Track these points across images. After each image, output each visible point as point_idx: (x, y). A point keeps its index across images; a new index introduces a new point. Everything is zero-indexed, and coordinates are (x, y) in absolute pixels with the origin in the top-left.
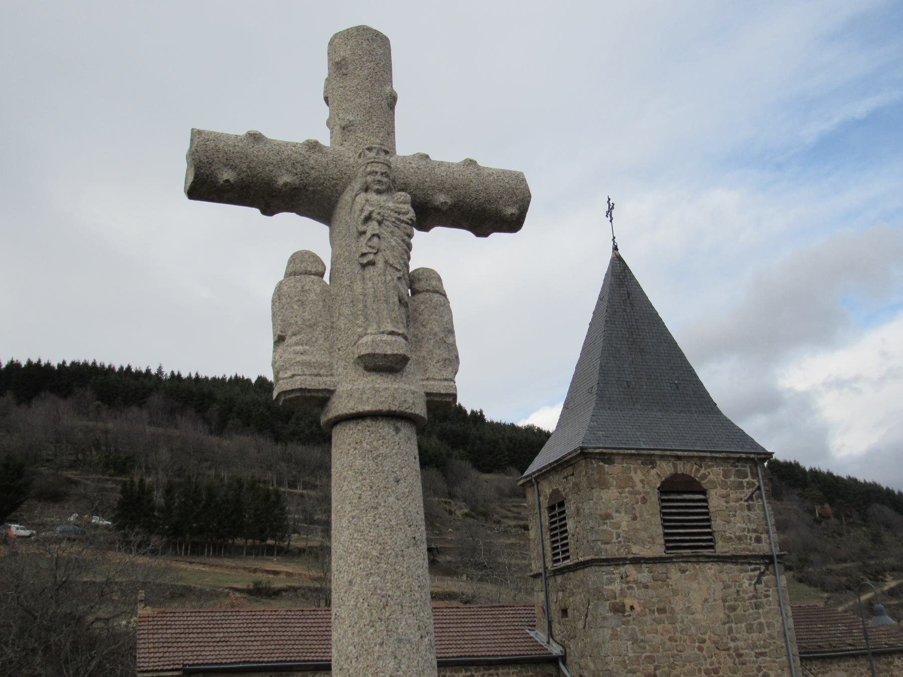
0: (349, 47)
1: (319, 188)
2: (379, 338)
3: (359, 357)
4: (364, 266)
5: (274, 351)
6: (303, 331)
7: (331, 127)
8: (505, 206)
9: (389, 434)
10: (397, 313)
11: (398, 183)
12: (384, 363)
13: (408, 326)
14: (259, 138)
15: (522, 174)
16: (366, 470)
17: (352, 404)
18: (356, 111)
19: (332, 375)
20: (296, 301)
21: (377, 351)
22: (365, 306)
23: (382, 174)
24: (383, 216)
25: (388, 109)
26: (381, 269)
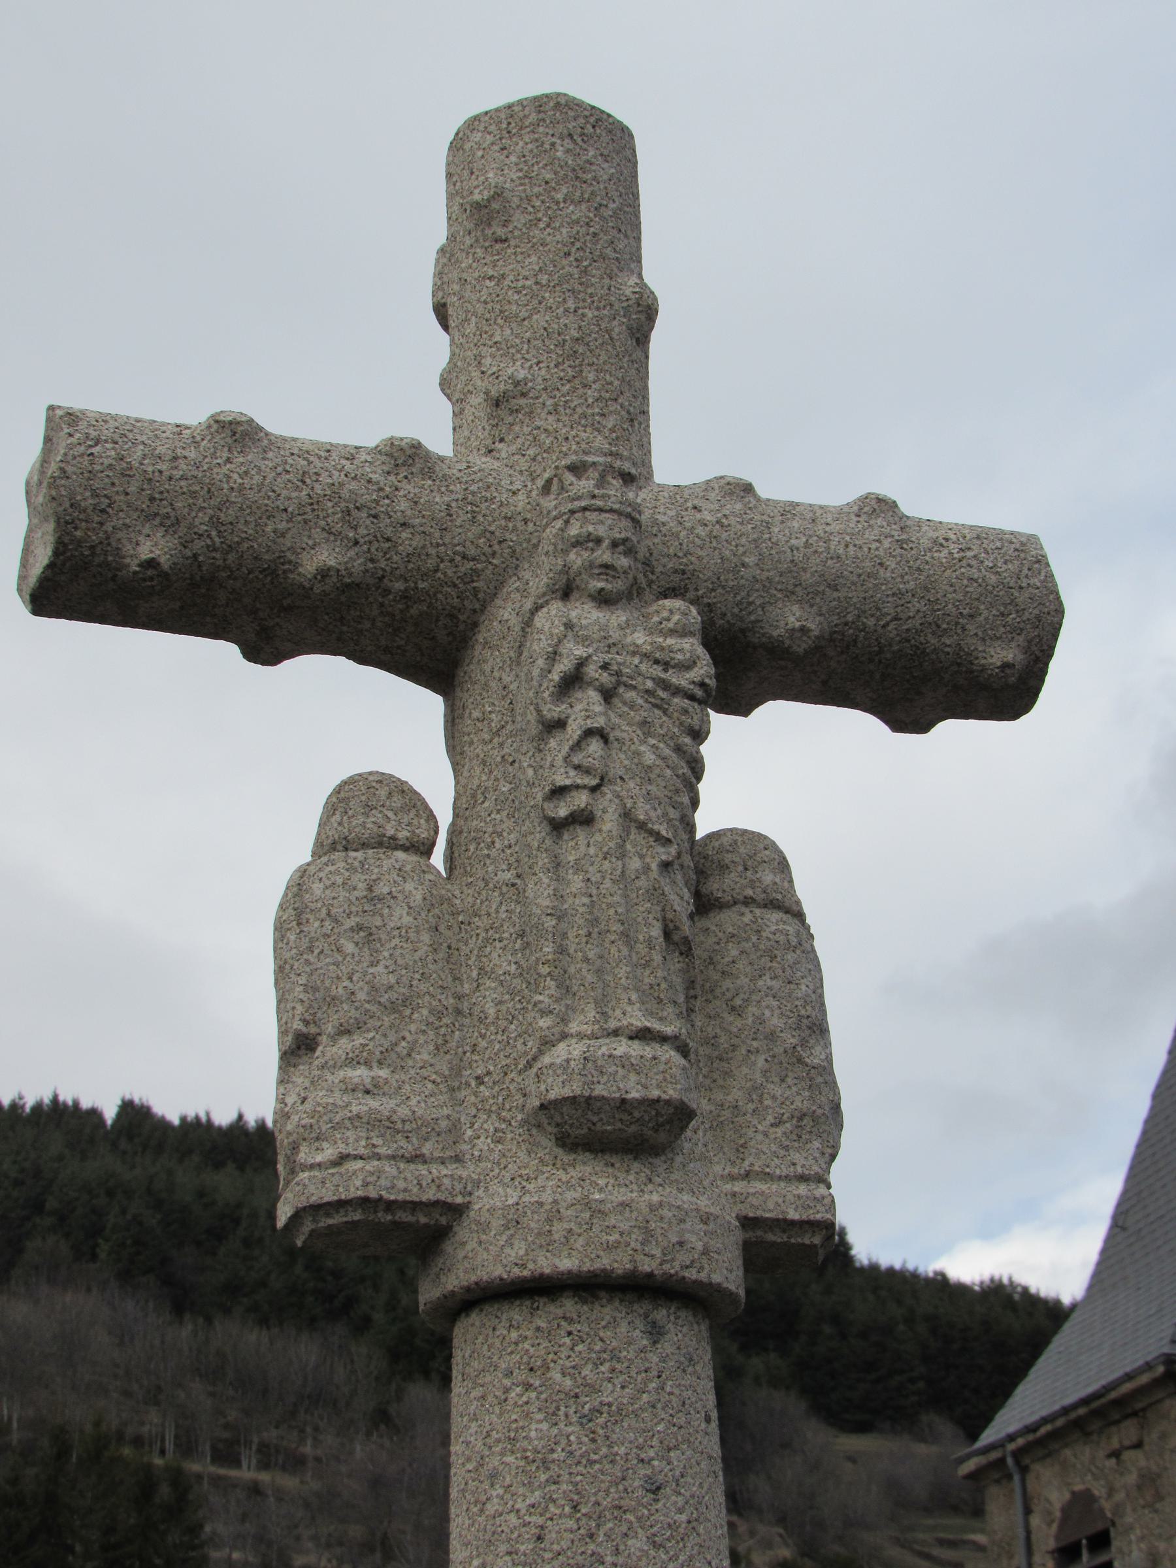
0: (513, 159)
1: (421, 585)
2: (604, 1049)
3: (542, 1107)
4: (558, 827)
5: (281, 1082)
6: (372, 1023)
7: (457, 396)
8: (983, 640)
9: (629, 1343)
10: (660, 974)
11: (659, 569)
12: (619, 1125)
13: (691, 1010)
14: (245, 434)
15: (1033, 540)
16: (559, 1455)
17: (519, 1249)
18: (534, 352)
19: (458, 1159)
20: (352, 929)
21: (599, 1091)
22: (562, 950)
23: (615, 544)
24: (618, 674)
25: (631, 343)
26: (611, 838)
